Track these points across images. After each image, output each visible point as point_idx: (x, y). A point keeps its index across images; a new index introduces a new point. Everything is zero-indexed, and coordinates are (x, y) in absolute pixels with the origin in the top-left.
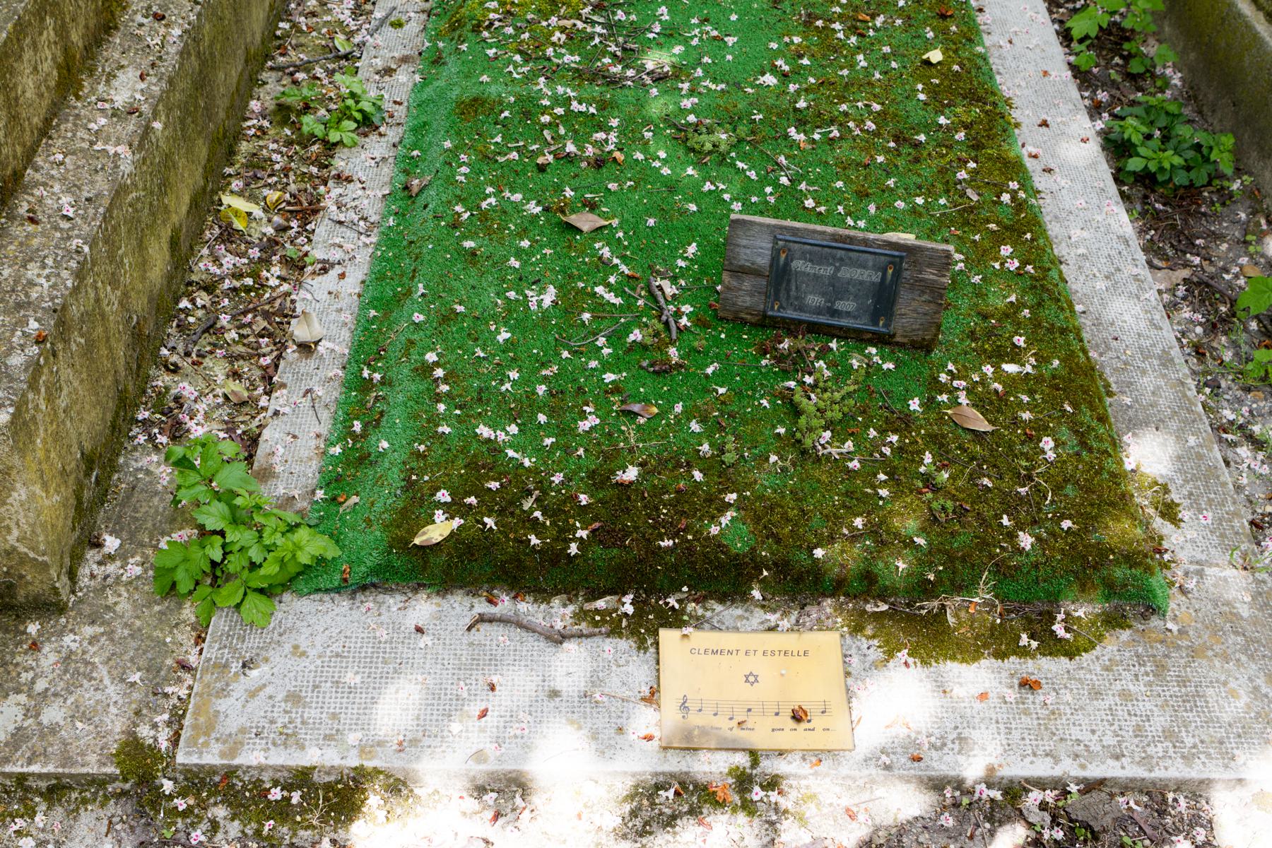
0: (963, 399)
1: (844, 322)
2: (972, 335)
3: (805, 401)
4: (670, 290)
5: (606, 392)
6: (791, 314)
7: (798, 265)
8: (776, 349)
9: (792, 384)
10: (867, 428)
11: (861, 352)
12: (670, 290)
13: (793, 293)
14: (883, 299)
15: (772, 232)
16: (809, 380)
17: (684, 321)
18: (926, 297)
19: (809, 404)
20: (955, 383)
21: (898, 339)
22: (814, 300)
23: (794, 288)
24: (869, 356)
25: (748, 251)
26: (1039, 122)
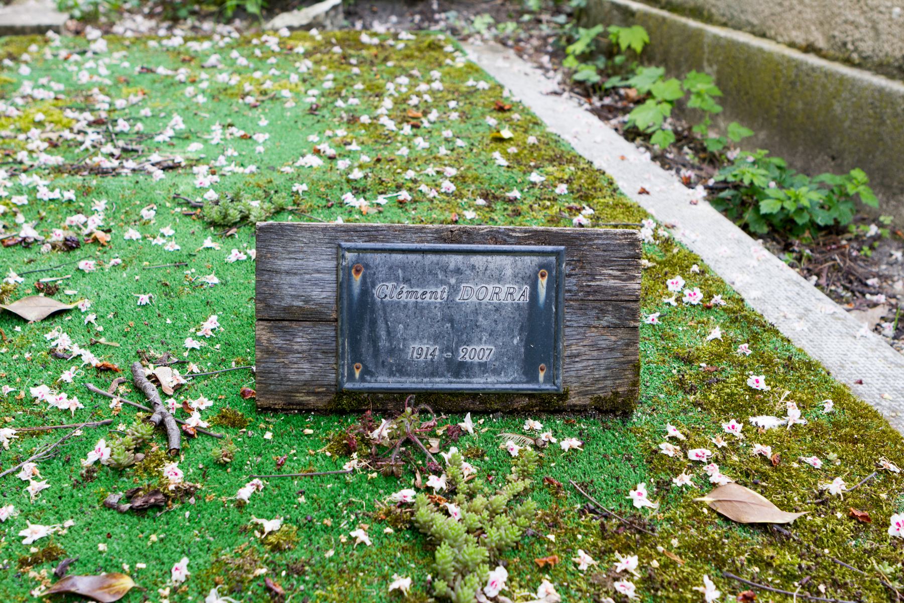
0: (716, 474)
1: (479, 383)
2: (681, 384)
3: (439, 517)
4: (169, 377)
5: (23, 563)
6: (385, 381)
7: (386, 291)
8: (368, 443)
9: (408, 494)
10: (569, 551)
11: (518, 429)
12: (169, 377)
13: (383, 343)
14: (539, 333)
15: (333, 240)
16: (437, 483)
17: (194, 421)
18: (608, 319)
19: (452, 521)
20: (692, 454)
21: (574, 400)
22: (421, 350)
23: (383, 334)
24: (532, 433)
25: (295, 280)
26: (639, 189)
